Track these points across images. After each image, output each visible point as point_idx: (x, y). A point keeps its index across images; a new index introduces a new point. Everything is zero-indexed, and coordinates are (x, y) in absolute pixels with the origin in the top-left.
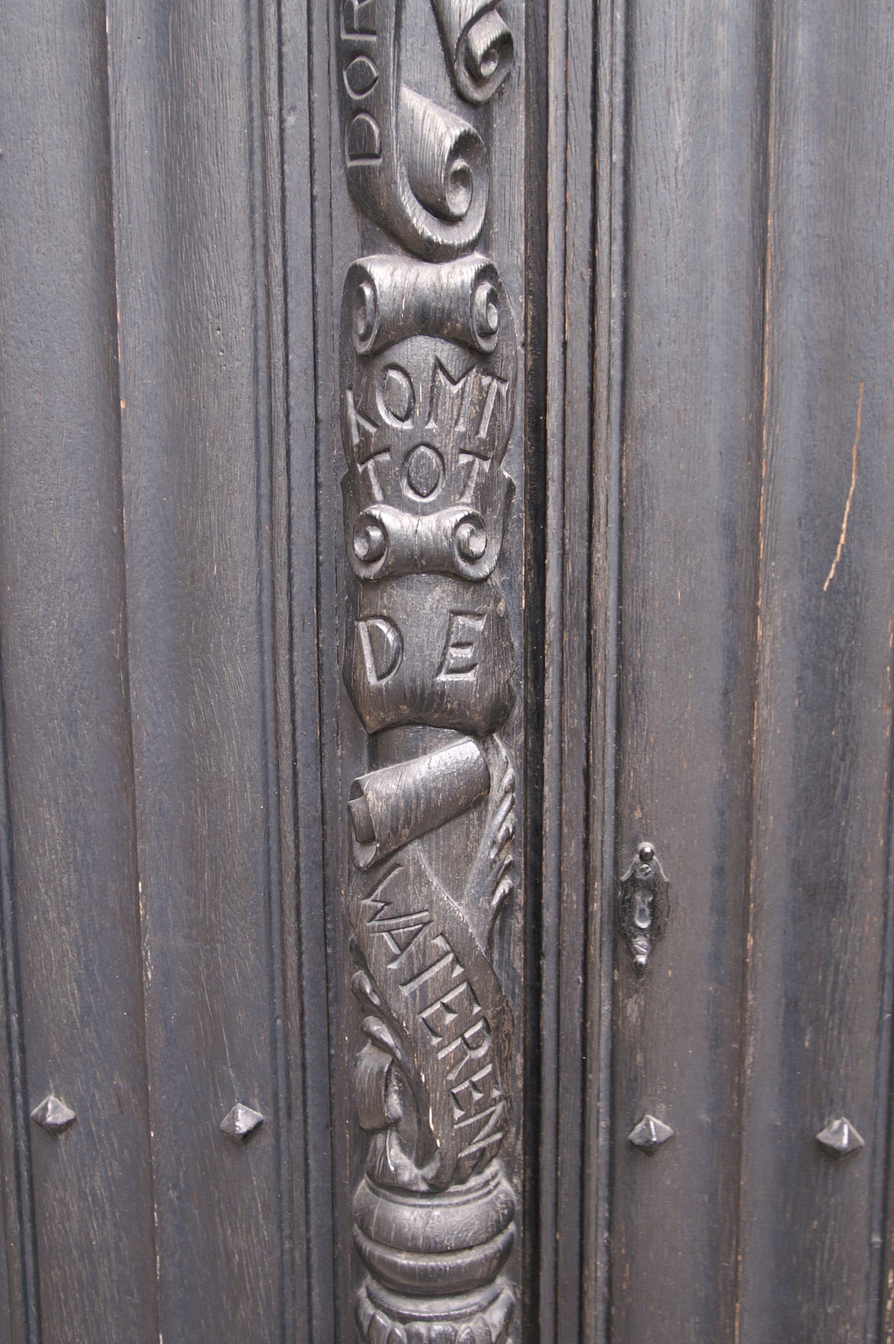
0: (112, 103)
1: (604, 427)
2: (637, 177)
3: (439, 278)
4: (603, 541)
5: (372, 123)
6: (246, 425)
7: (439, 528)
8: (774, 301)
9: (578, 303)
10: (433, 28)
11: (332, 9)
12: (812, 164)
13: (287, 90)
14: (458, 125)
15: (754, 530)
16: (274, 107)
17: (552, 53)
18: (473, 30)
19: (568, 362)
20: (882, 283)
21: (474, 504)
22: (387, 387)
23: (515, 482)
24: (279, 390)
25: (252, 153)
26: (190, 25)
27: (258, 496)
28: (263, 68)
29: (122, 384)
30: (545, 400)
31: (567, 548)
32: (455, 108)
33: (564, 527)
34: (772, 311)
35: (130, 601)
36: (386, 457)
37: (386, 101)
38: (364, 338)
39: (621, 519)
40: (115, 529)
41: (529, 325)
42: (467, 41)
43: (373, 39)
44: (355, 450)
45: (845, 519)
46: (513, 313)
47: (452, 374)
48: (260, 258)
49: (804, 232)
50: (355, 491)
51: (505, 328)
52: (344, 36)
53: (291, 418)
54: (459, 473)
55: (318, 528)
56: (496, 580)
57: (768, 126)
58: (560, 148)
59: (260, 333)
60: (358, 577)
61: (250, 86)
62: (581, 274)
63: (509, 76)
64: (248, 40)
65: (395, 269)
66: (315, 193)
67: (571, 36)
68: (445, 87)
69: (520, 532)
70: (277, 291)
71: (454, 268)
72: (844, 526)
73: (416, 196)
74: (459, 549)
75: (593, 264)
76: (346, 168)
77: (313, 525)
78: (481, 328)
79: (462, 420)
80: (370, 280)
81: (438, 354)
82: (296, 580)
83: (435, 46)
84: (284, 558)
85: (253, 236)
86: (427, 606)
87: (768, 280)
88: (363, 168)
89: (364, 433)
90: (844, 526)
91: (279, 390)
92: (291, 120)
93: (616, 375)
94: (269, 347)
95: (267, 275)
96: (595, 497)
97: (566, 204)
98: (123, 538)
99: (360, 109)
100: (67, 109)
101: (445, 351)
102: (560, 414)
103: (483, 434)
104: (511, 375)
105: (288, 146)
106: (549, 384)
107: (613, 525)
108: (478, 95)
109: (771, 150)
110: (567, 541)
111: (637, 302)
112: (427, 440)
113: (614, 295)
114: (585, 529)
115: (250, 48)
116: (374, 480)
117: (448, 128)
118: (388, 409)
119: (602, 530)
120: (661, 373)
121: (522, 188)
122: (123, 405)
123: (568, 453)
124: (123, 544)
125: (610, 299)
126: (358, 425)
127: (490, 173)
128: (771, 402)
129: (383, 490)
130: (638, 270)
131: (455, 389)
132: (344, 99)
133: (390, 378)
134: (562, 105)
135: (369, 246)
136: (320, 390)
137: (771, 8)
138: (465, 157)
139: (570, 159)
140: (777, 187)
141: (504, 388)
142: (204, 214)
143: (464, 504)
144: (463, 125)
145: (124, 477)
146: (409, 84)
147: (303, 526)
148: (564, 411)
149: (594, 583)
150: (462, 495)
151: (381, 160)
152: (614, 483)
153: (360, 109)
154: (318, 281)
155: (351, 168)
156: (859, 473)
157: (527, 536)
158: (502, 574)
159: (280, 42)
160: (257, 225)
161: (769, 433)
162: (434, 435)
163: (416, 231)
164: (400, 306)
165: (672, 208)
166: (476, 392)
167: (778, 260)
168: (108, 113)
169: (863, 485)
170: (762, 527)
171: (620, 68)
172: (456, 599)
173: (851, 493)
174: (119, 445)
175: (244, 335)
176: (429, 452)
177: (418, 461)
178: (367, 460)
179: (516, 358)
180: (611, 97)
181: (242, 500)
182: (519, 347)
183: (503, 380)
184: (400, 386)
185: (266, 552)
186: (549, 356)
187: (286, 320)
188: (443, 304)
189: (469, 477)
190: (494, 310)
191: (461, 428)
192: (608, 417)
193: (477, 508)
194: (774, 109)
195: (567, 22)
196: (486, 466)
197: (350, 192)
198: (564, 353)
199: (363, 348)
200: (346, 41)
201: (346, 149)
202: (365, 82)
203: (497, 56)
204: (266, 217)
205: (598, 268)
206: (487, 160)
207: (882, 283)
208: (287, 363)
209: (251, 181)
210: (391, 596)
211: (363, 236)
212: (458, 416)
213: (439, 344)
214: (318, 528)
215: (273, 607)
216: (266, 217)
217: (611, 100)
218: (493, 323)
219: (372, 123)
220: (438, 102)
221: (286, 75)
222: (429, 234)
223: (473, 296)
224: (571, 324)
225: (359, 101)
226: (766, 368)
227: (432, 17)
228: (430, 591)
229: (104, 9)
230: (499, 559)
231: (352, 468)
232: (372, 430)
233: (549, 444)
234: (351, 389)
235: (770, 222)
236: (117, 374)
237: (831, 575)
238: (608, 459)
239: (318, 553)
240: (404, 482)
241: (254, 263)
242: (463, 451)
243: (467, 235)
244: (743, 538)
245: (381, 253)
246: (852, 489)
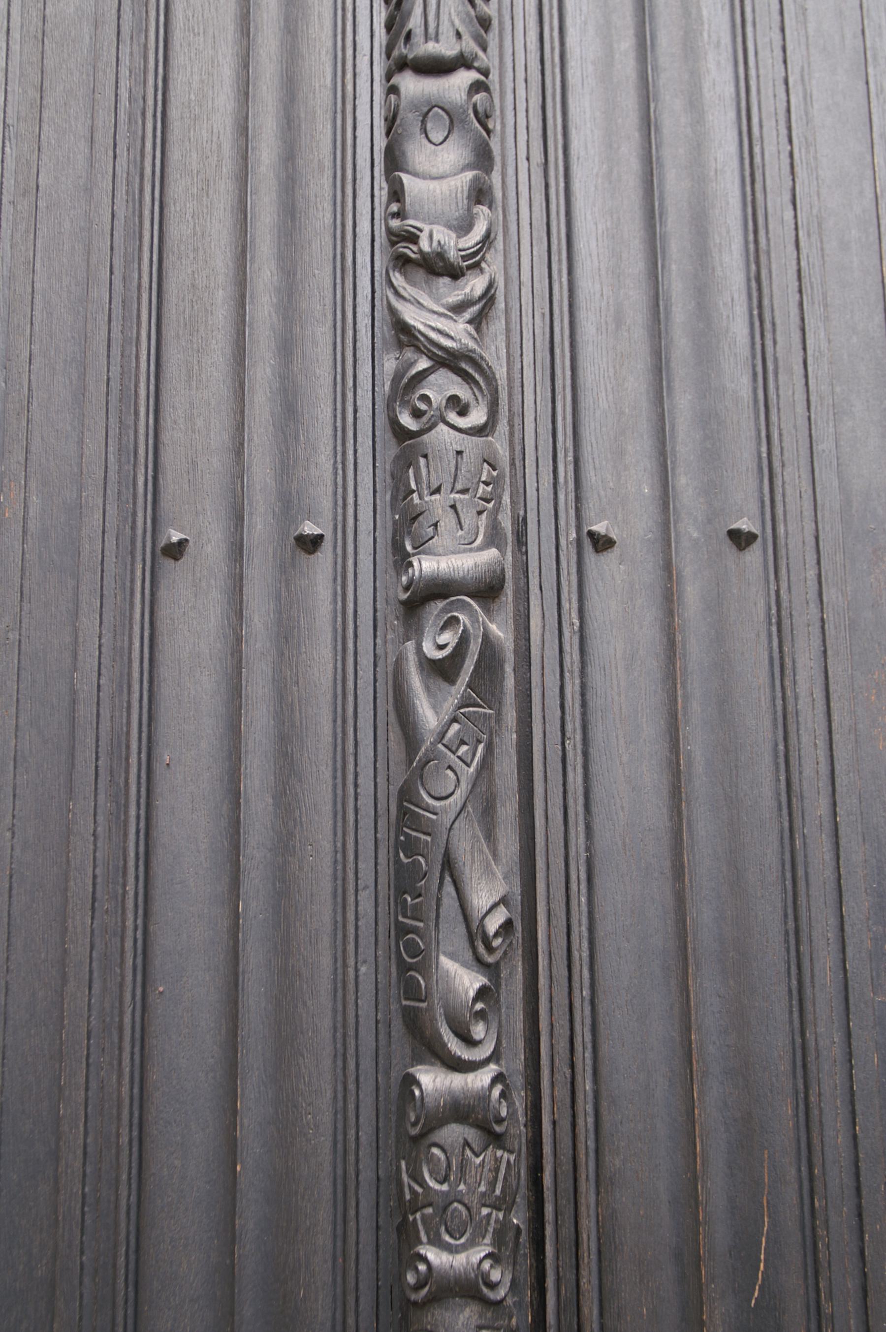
0: (241, 957)
1: (584, 1184)
2: (600, 1006)
3: (466, 1084)
4: (587, 1269)
5: (420, 979)
6: (327, 1183)
7: (468, 1263)
8: (699, 1093)
9: (562, 1093)
10: (460, 918)
11: (392, 899)
12: (720, 997)
13: (360, 950)
14: (478, 981)
15: (698, 1260)
16: (351, 962)
17: (539, 923)
18: (487, 919)
19: (557, 1136)
20: (774, 1079)
21: (493, 1244)
22: (430, 1159)
23: (522, 1226)
24: (352, 1158)
25: (335, 991)
26: (296, 907)
27: (335, 1236)
28: (345, 936)
29: (239, 1153)
30: (542, 1163)
31: (561, 1274)
32: (476, 969)
33: (558, 1258)
34: (699, 1099)
35: (236, 1318)
36: (429, 1210)
37: (430, 966)
38: (414, 1124)
39: (599, 1252)
40: (228, 1262)
41: (529, 1107)
42: (483, 926)
43: (421, 925)
44: (407, 1204)
45: (763, 1252)
46: (517, 1104)
47: (476, 1150)
48: (340, 1063)
49: (718, 1043)
50: (406, 1236)
51: (512, 1114)
52: (401, 919)
53: (360, 1178)
54: (482, 1221)
55: (378, 1260)
56: (509, 1301)
57: (687, 972)
58: (547, 986)
59: (339, 1116)
60: (409, 1300)
61: (335, 947)
62: (564, 1073)
63: (511, 943)
64: (335, 917)
65: (436, 1078)
66: (378, 1018)
67: (552, 913)
68: (469, 955)
69: (526, 1262)
70: (352, 1087)
71: (476, 1076)
72: (762, 1257)
73: (450, 1028)
74: (483, 1279)
75: (572, 1066)
76: (401, 1004)
77: (375, 1259)
78: (495, 1117)
79: (483, 1183)
80: (419, 1085)
81: (466, 1136)
82: (362, 1300)
83: (461, 929)
84: (353, 1284)
85: (335, 1048)
86: (460, 1323)
87: (695, 1077)
88: (414, 1007)
89: (413, 1191)
90: (762, 1257)
91: (352, 1158)
92: (363, 969)
93: (591, 1144)
94: (345, 1127)
95: (345, 1075)
96: (580, 1236)
97: (552, 1025)
98: (234, 1268)
99: (411, 968)
100: (209, 960)
101: (471, 1134)
102: (553, 1173)
103: (498, 1192)
104: (517, 1148)
105: (361, 987)
106: (544, 1152)
107: (594, 1257)
108: (490, 959)
109: (691, 988)
110: (561, 1269)
111: (604, 1094)
112: (459, 1198)
113: (587, 1088)
114: (574, 1260)
115: (336, 922)
116: (421, 1227)
117: (472, 984)
118: (431, 1176)
119: (586, 1260)
120: (623, 1144)
121: (522, 1017)
122: (238, 1168)
123: (559, 1202)
124: (234, 1273)
125: (585, 1090)
126: (409, 1186)
127: (499, 1009)
128: (703, 1164)
129: (428, 1234)
130: (604, 1070)
131: (478, 1161)
132: (400, 961)
133: (433, 1154)
134: (547, 957)
135: (418, 1059)
136: (381, 1157)
137: (684, 896)
138: (483, 1001)
139: (554, 994)
140: (696, 1013)
141: (512, 1158)
142: (302, 1033)
143: (485, 1245)
144: (481, 980)
145: (237, 1222)
146: (445, 954)
147: (368, 1258)
148: (555, 1172)
149: (581, 1302)
150: (484, 1237)
151: (426, 1004)
152: (593, 1224)
153: (411, 968)
154: (380, 1079)
155: (405, 1005)
156: (769, 1217)
157: (531, 1265)
158: (513, 1296)
159: (357, 919)
160: (338, 1041)
161: (702, 1187)
162: (463, 1195)
163: (451, 1052)
164: (440, 1103)
165: (625, 1028)
166: (493, 1163)
167: (701, 1064)
168: (237, 964)
169: (773, 1225)
170: (703, 1257)
171: (585, 934)
172: (480, 1317)
173: (765, 1232)
174: (234, 1198)
175: (327, 1118)
176: (460, 1207)
177: (452, 1214)
178: (416, 1211)
179: (520, 1135)
180: (581, 952)
181: (323, 1240)
182: (522, 1128)
183: (511, 1152)
184: (439, 1159)
185: (339, 1279)
186: (544, 1131)
187: (357, 1107)
188: (469, 1103)
189: (488, 1223)
190: (504, 1103)
191: (482, 1188)
192: (587, 1176)
193: (494, 1247)
194: (691, 961)
195: (549, 903)
196: (501, 1215)
197: (404, 1021)
198: (554, 1129)
199: (414, 1131)
200: (402, 922)
201: (402, 992)
202: (415, 952)
203: (503, 933)
204: (345, 1035)
205: (576, 1070)
206: (498, 1001)
207: (774, 1079)
208: (357, 1138)
209: (334, 1010)
210: (433, 1315)
211: (413, 1051)
212: (481, 1180)
213: (466, 1129)
214: (378, 1260)
215: (344, 1322)
216: (345, 1035)
217: (580, 955)
218: (504, 1113)
219: (420, 979)
220: (465, 965)
221: (360, 940)
222: (459, 1054)
223: (490, 1096)
224: (558, 1109)
225: (411, 963)
226: (698, 1140)
227: (460, 910)
228: (462, 1311)
229: (238, 896)
230: (511, 1285)
231: (405, 1218)
232: (420, 1190)
233: (545, 1195)
234: (404, 1158)
235: (693, 1037)
236: (236, 1146)
237: (756, 1295)
238: (588, 1207)
239: (378, 1280)
240: (443, 1229)
241: (336, 1066)
242: (484, 1205)
243: (485, 1053)
244: (689, 1261)
245: (425, 1064)
246: (765, 1229)
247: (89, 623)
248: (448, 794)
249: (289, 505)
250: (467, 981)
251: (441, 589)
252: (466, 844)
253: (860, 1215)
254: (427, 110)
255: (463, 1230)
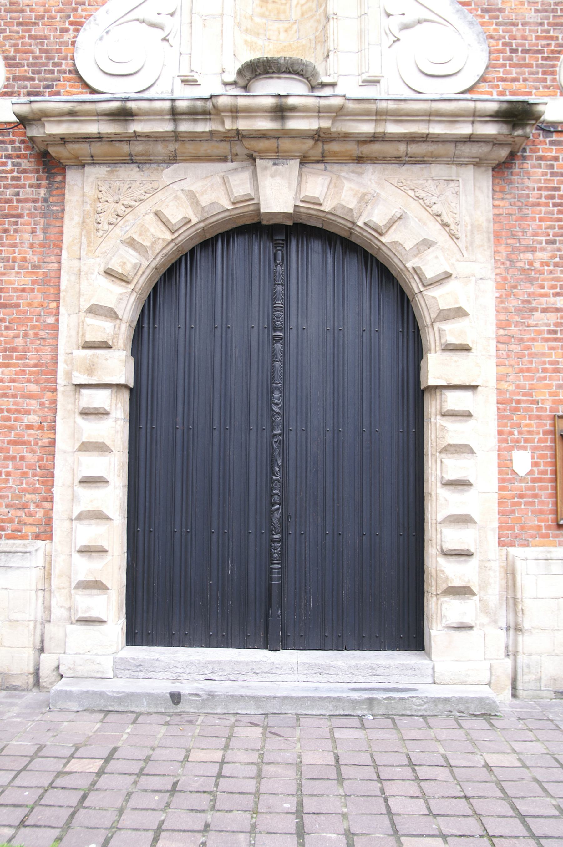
181: (256, 283)
247: (243, 436)
248: (276, 454)
249: (262, 426)
250: (278, 469)
251: (276, 435)
252: (278, 457)
253: (125, 774)
254: (276, 387)
255: (277, 489)
